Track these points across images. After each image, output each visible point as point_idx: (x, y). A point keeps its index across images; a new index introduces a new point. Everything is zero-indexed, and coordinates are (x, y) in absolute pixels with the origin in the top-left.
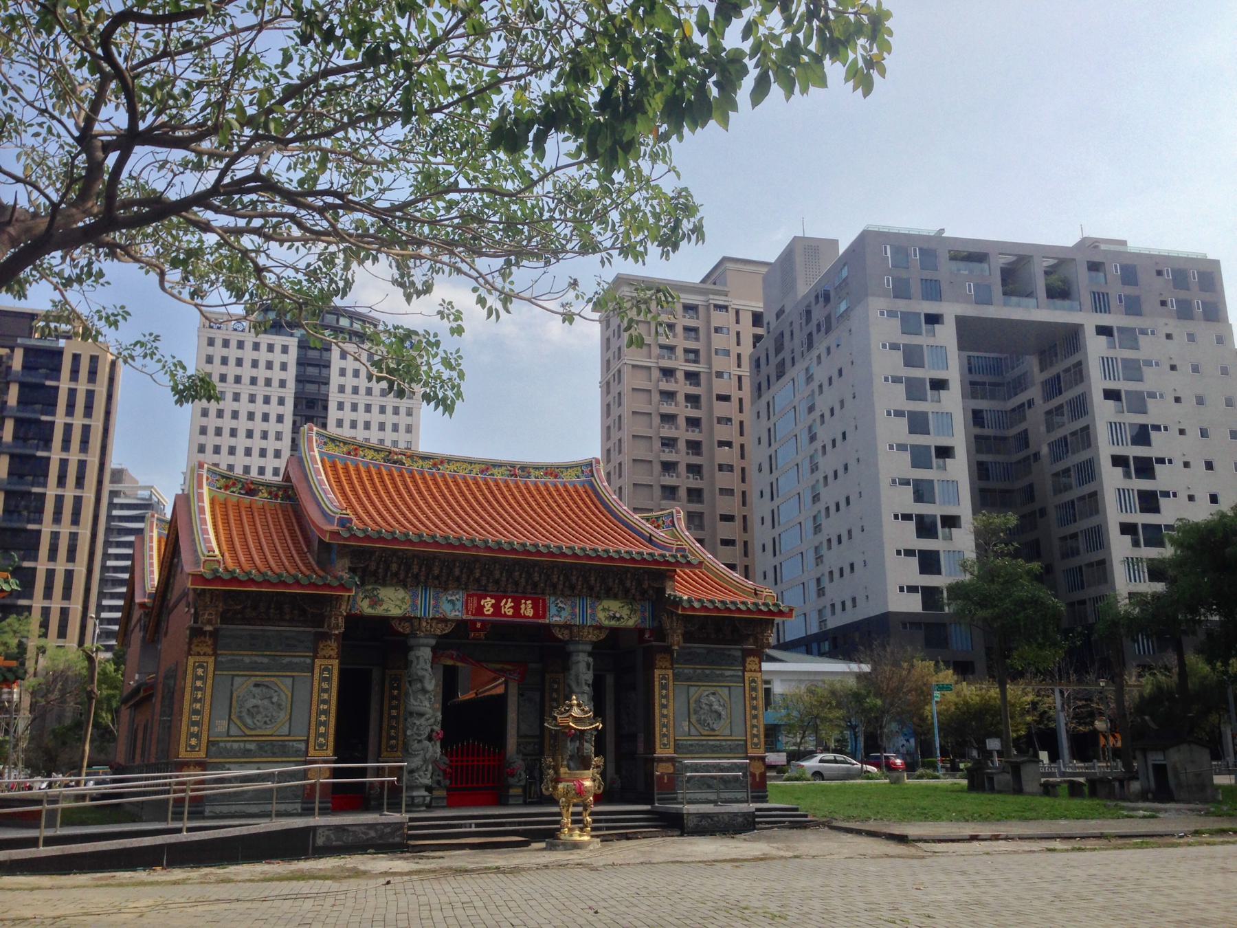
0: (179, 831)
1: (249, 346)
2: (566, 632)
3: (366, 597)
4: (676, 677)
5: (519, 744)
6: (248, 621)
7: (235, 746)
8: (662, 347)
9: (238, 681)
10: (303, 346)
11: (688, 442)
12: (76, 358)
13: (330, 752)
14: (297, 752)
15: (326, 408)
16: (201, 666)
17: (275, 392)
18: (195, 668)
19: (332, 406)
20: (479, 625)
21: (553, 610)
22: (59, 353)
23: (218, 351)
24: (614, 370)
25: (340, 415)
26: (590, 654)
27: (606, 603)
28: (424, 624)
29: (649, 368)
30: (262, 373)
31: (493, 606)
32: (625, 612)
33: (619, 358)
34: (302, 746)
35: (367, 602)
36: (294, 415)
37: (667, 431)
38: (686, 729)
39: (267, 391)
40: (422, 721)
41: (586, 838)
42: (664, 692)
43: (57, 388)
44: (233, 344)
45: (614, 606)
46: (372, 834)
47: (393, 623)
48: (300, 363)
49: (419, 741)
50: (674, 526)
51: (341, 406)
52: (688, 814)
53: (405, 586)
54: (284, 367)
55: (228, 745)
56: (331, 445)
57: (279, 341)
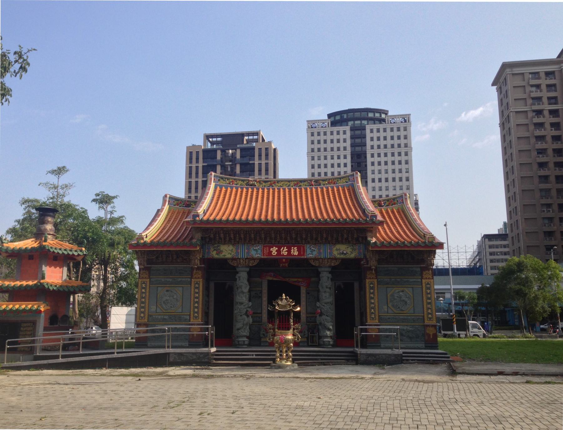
0: (113, 353)
1: (328, 133)
2: (317, 262)
3: (215, 250)
4: (379, 283)
5: (307, 317)
6: (163, 263)
7: (160, 317)
8: (533, 99)
9: (159, 289)
10: (352, 129)
11: (554, 150)
12: (260, 149)
13: (200, 320)
14: (185, 320)
15: (366, 157)
16: (144, 283)
17: (342, 153)
18: (142, 284)
19: (369, 156)
20: (284, 260)
21: (309, 251)
22: (253, 148)
23: (316, 138)
24: (505, 116)
25: (372, 160)
26: (330, 273)
27: (338, 246)
28: (242, 261)
29: (526, 111)
30: (335, 145)
31: (276, 251)
32: (349, 250)
33: (508, 109)
34: (188, 317)
35: (215, 252)
36: (352, 162)
37: (540, 145)
38: (386, 310)
39: (386, 151)
40: (242, 306)
41: (289, 363)
42: (372, 291)
43: (254, 164)
44: (322, 134)
45: (343, 248)
46: (194, 357)
47: (228, 261)
48: (352, 137)
49: (241, 315)
50: (403, 203)
51: (372, 156)
52: (361, 354)
53: (233, 245)
54: (372, 139)
55: (157, 317)
56: (221, 180)
57: (341, 129)
